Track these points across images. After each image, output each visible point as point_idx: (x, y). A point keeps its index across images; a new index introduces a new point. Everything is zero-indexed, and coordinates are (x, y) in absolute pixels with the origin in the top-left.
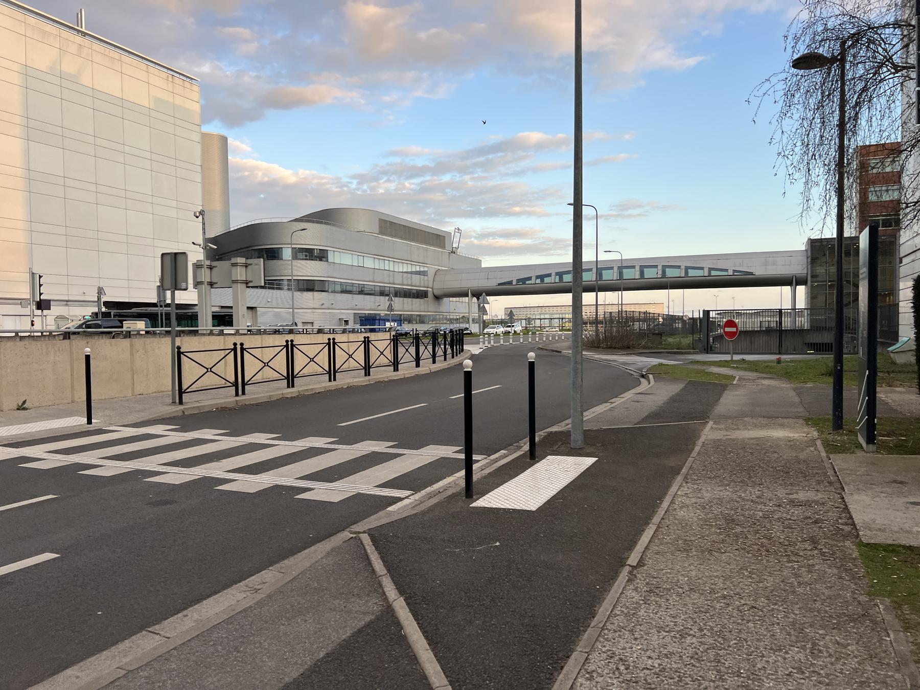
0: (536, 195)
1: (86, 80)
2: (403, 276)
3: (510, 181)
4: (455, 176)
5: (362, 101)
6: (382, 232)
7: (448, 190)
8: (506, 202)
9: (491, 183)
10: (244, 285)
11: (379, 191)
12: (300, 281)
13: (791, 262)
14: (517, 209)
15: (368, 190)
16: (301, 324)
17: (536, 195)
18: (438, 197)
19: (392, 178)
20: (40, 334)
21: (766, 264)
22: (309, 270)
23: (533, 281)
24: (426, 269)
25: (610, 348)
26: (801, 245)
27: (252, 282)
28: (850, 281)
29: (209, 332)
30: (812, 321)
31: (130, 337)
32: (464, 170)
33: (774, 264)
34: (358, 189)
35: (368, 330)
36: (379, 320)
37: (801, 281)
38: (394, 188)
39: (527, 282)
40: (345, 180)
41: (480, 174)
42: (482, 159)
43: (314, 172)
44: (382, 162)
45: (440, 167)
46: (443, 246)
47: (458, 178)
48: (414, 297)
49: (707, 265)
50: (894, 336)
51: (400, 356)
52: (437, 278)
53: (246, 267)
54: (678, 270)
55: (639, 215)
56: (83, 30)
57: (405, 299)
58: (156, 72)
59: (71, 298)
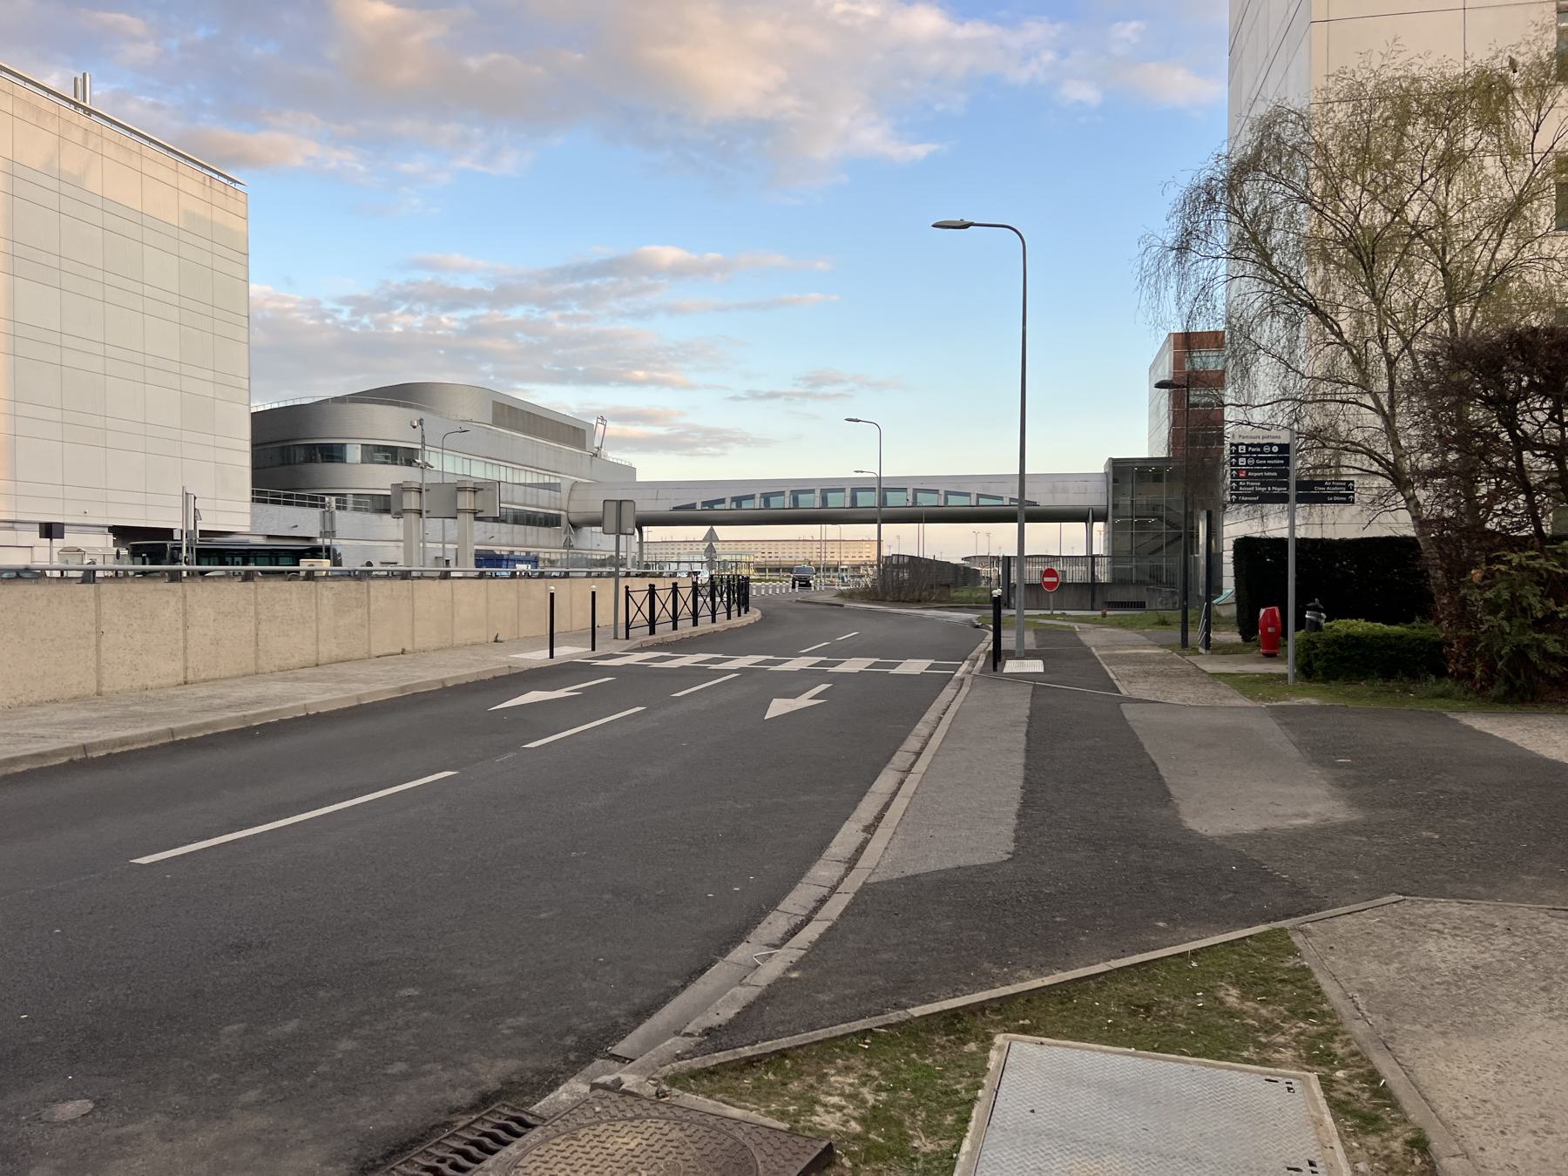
0: (672, 354)
1: (93, 184)
2: (525, 492)
3: (626, 325)
4: (533, 311)
5: (361, 168)
6: (496, 422)
7: (519, 335)
8: (621, 362)
9: (593, 327)
10: (472, 516)
11: (392, 329)
12: (376, 498)
13: (1086, 490)
14: (640, 374)
15: (372, 326)
16: (378, 564)
17: (672, 354)
18: (502, 344)
19: (416, 308)
20: (57, 574)
21: (1053, 491)
22: (384, 478)
23: (727, 505)
24: (558, 481)
25: (898, 601)
26: (1099, 467)
27: (482, 511)
28: (1162, 517)
29: (585, 574)
30: (1114, 572)
31: (94, 582)
32: (547, 302)
33: (1065, 491)
34: (353, 323)
35: (196, 573)
36: (507, 560)
37: (1100, 516)
38: (420, 325)
39: (716, 507)
40: (328, 305)
41: (577, 311)
42: (578, 285)
43: (269, 288)
44: (398, 279)
45: (504, 295)
46: (582, 446)
47: (536, 313)
48: (540, 525)
49: (975, 490)
50: (1220, 591)
51: (699, 606)
52: (575, 496)
53: (475, 492)
54: (935, 496)
55: (839, 395)
56: (87, 104)
57: (529, 527)
58: (188, 171)
59: (20, 518)
